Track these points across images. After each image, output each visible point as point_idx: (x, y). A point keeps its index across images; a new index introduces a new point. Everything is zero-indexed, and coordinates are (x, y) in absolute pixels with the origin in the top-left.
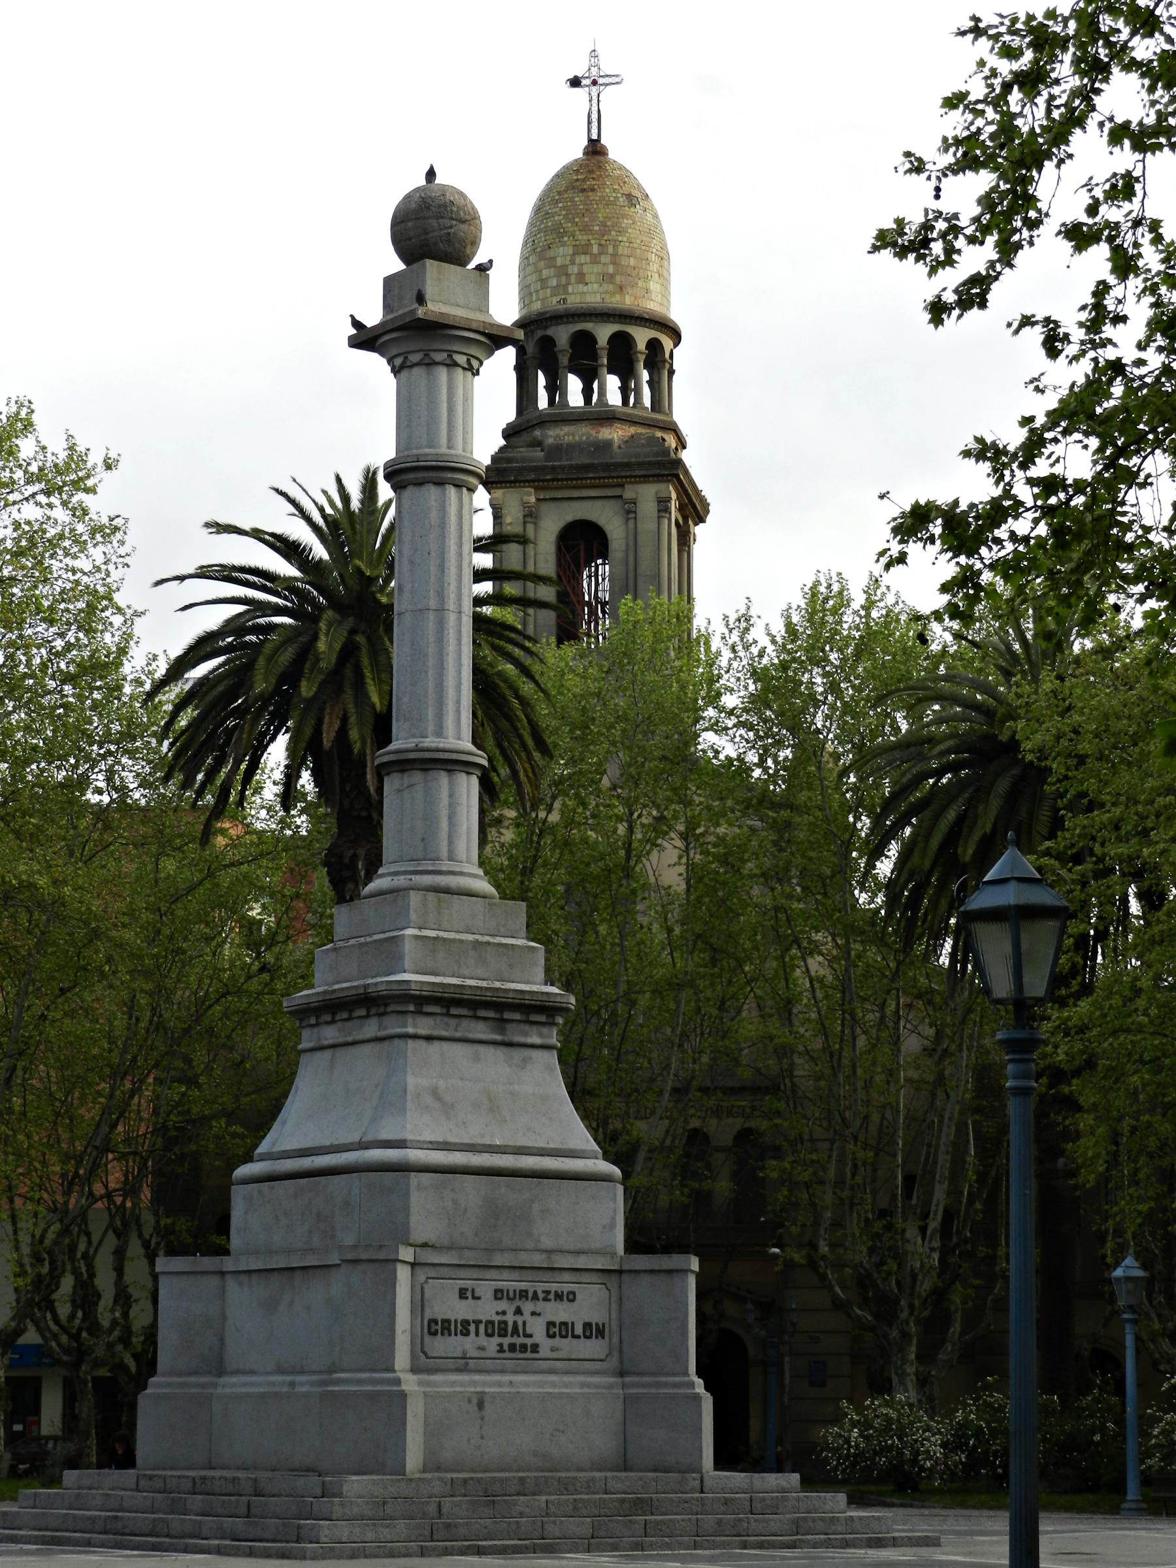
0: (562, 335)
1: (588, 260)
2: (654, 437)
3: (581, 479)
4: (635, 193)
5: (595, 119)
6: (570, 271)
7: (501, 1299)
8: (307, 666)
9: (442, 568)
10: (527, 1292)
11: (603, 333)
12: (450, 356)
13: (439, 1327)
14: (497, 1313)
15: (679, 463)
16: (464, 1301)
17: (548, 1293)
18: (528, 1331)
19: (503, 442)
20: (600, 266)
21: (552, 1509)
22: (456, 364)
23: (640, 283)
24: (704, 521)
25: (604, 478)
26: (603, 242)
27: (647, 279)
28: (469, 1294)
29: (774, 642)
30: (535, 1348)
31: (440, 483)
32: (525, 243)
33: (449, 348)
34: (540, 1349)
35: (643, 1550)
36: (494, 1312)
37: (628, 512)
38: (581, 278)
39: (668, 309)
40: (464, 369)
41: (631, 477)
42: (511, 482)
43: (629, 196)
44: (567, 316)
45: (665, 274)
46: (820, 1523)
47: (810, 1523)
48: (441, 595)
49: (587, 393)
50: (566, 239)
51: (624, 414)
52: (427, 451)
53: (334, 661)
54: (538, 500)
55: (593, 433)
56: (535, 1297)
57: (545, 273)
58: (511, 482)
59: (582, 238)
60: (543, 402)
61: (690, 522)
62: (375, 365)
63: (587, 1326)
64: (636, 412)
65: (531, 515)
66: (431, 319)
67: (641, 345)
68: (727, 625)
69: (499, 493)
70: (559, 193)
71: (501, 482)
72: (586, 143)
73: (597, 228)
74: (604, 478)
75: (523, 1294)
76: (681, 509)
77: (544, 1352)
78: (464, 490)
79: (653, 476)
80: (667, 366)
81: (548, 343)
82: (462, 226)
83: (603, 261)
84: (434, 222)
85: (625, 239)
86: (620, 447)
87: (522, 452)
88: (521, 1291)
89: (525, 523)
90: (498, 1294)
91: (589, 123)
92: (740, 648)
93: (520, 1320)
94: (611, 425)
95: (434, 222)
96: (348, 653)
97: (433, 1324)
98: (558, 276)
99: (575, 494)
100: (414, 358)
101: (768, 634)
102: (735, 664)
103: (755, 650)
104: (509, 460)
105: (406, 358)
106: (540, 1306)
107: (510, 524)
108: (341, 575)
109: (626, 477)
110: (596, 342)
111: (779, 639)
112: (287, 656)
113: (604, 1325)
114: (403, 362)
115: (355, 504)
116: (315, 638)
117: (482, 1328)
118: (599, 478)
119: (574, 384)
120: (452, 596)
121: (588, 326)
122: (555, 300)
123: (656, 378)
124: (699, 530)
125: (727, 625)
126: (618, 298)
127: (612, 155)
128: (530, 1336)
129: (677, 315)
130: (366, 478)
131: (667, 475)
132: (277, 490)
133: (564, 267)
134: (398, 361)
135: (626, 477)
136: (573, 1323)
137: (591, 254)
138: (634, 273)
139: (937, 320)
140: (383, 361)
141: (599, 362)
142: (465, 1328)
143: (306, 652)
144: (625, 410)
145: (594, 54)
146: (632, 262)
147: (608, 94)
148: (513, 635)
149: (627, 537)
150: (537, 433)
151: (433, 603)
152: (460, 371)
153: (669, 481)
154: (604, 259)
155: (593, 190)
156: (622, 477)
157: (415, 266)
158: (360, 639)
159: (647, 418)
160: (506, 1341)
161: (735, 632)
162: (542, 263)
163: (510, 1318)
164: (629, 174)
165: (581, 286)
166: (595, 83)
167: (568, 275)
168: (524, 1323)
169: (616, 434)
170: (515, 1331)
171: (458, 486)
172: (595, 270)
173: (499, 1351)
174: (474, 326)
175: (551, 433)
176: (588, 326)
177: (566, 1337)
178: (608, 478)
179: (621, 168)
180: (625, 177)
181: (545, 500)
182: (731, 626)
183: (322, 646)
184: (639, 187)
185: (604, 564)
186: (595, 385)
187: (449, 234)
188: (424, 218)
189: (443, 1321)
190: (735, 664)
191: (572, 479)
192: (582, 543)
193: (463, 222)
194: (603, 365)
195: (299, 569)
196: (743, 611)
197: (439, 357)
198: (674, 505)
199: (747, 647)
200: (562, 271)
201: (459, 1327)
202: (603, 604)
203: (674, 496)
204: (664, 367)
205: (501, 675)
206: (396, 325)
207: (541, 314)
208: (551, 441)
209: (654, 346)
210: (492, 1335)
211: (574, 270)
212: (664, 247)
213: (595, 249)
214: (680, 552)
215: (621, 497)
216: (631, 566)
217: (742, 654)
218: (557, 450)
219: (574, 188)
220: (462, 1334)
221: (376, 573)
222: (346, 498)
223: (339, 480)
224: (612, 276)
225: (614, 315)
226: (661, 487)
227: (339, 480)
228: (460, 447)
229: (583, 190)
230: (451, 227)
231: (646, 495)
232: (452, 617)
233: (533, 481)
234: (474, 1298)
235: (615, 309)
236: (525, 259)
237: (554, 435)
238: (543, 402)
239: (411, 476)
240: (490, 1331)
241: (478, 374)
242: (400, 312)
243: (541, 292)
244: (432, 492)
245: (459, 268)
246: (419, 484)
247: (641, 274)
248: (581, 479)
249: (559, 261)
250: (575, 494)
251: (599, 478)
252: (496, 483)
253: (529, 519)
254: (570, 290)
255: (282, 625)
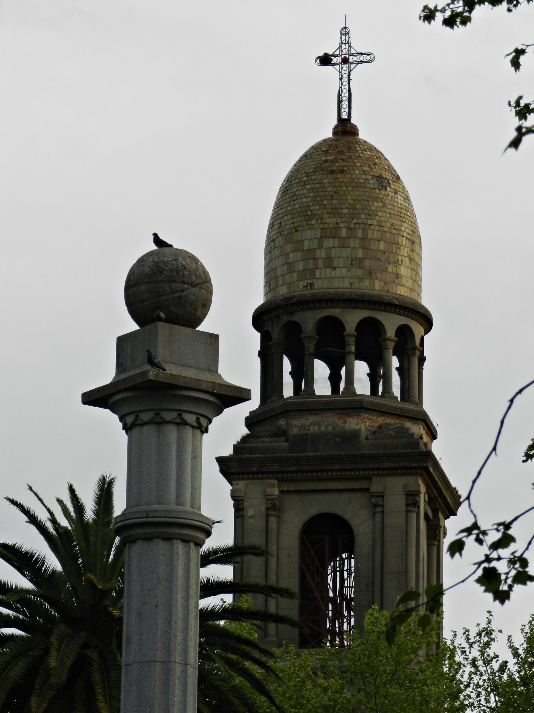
0: (309, 320)
1: (336, 245)
2: (402, 428)
3: (327, 471)
4: (387, 175)
5: (345, 98)
6: (317, 256)
8: (38, 681)
9: (169, 621)
11: (352, 319)
12: (180, 415)
15: (429, 456)
19: (246, 431)
20: (349, 250)
22: (185, 423)
23: (390, 268)
24: (455, 514)
25: (350, 470)
26: (352, 226)
27: (397, 263)
29: (516, 654)
31: (168, 539)
32: (272, 225)
33: (180, 408)
37: (375, 506)
38: (329, 263)
39: (419, 295)
40: (193, 427)
41: (378, 469)
42: (253, 473)
43: (380, 178)
44: (314, 301)
45: (416, 258)
48: (168, 647)
49: (334, 379)
50: (313, 222)
51: (372, 403)
52: (156, 507)
53: (65, 677)
54: (282, 492)
55: (340, 423)
57: (292, 257)
58: (253, 473)
59: (330, 221)
60: (288, 391)
61: (441, 516)
62: (108, 419)
64: (384, 401)
65: (274, 508)
66: (162, 380)
67: (391, 333)
68: (468, 639)
69: (241, 484)
70: (307, 174)
71: (243, 474)
72: (335, 122)
73: (345, 211)
74: (350, 470)
76: (431, 502)
78: (192, 545)
79: (402, 468)
80: (418, 353)
81: (294, 329)
82: (193, 289)
83: (352, 245)
84: (167, 287)
85: (375, 223)
86: (367, 438)
87: (266, 442)
89: (268, 516)
91: (340, 101)
92: (480, 663)
94: (359, 415)
95: (167, 287)
96: (80, 668)
98: (305, 260)
99: (320, 486)
100: (145, 417)
101: (510, 647)
102: (476, 679)
103: (496, 665)
104: (252, 451)
105: (137, 416)
107: (252, 517)
108: (74, 587)
109: (373, 469)
110: (344, 329)
111: (521, 651)
112: (17, 671)
114: (135, 421)
115: (89, 514)
116: (46, 652)
118: (345, 470)
119: (321, 370)
120: (179, 649)
121: (336, 312)
122: (302, 284)
123: (406, 365)
125: (468, 639)
126: (367, 283)
127: (362, 135)
129: (427, 301)
130: (101, 488)
131: (416, 468)
132: (13, 502)
133: (311, 250)
134: (130, 420)
135: (373, 469)
137: (340, 238)
138: (384, 258)
139: (488, 612)
140: (115, 418)
141: (347, 349)
143: (37, 667)
144: (375, 400)
145: (345, 31)
146: (382, 246)
147: (358, 72)
148: (248, 649)
149: (374, 532)
150: (282, 422)
151: (160, 656)
152: (189, 429)
153: (417, 474)
154: (353, 243)
155: (342, 172)
156: (369, 470)
157: (147, 327)
158: (93, 654)
159: (396, 408)
161: (476, 646)
162: (289, 247)
164: (379, 155)
165: (328, 270)
166: (345, 61)
167: (315, 259)
169: (362, 424)
171: (186, 541)
172: (344, 255)
174: (203, 386)
175: (296, 422)
176: (336, 312)
178: (355, 470)
179: (372, 148)
180: (374, 157)
181: (288, 492)
182: (472, 640)
183: (52, 662)
184: (390, 169)
185: (349, 558)
186: (343, 372)
187: (180, 297)
188: (158, 282)
190: (476, 679)
191: (317, 471)
192: (327, 537)
193: (194, 285)
194: (350, 353)
195: (31, 581)
196: (484, 625)
197: (169, 416)
198: (423, 499)
199: (487, 662)
200: (309, 255)
202: (349, 601)
203: (423, 489)
204: (414, 354)
205: (235, 690)
206: (128, 385)
207: (287, 299)
208: (295, 431)
209: (404, 332)
211: (321, 254)
212: (415, 231)
213: (344, 233)
214: (429, 546)
215: (367, 490)
216: (378, 563)
217: (482, 669)
218: (302, 440)
219: (322, 169)
221: (108, 586)
222: (79, 508)
223: (72, 490)
224: (361, 261)
225: (363, 301)
226: (411, 479)
227: (72, 490)
228: (188, 503)
229: (332, 172)
230: (183, 291)
231: (394, 488)
232: (178, 668)
233: (277, 472)
235: (363, 295)
236: (271, 242)
237: (298, 425)
238: (288, 391)
239: (140, 531)
241: (207, 431)
242: (133, 373)
243: (287, 276)
244: (160, 546)
245: (189, 330)
246: (148, 539)
247: (391, 260)
248: (327, 471)
249: (307, 245)
250: (320, 486)
251: (345, 470)
252: (238, 474)
253: (272, 512)
254: (317, 275)
255: (12, 637)
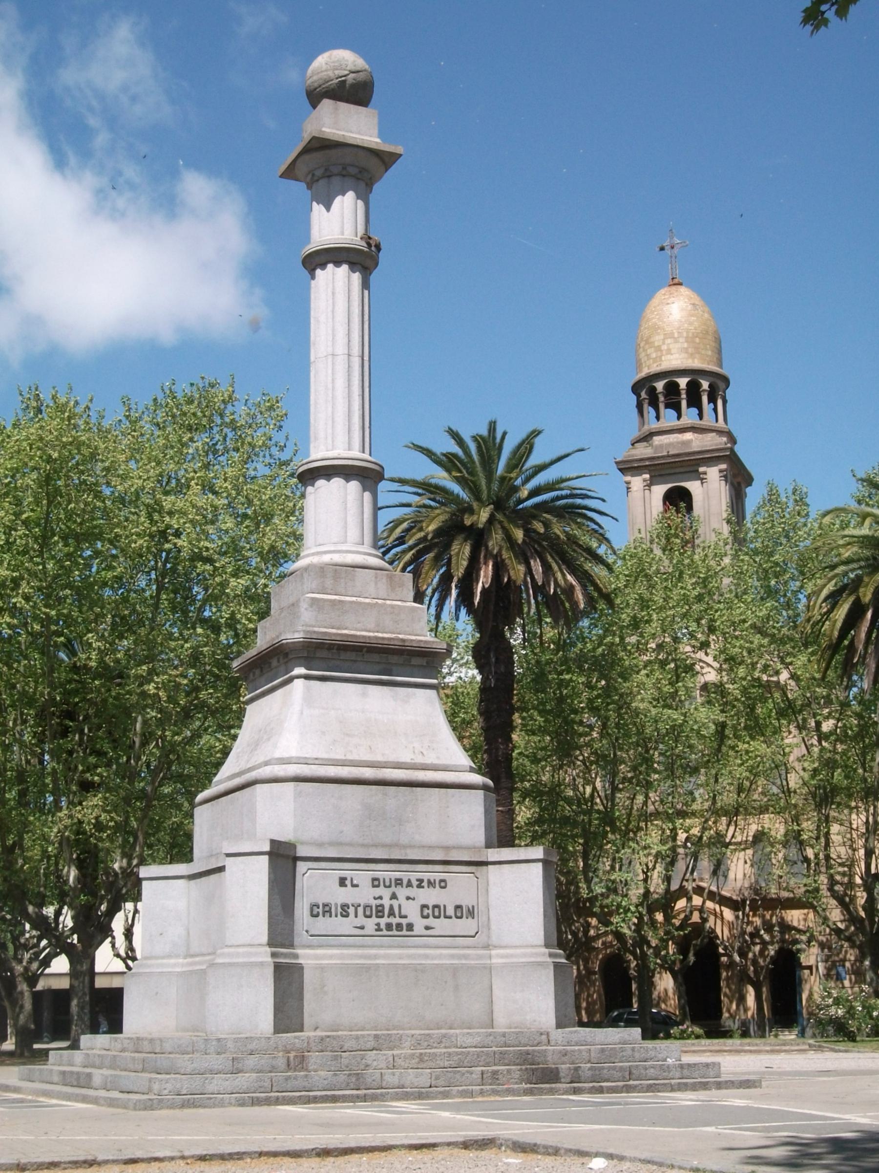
7: (378, 886)
10: (401, 880)
11: (683, 382)
13: (320, 910)
14: (375, 898)
16: (343, 888)
17: (421, 881)
18: (403, 913)
21: (399, 1062)
28: (348, 882)
30: (410, 927)
34: (414, 928)
35: (472, 1097)
36: (371, 897)
38: (669, 351)
46: (652, 1070)
47: (642, 1071)
56: (409, 884)
63: (458, 907)
75: (399, 882)
77: (418, 929)
81: (652, 392)
88: (396, 880)
90: (375, 882)
93: (395, 903)
97: (315, 908)
99: (672, 471)
106: (413, 892)
113: (473, 907)
117: (360, 910)
124: (748, 490)
128: (406, 917)
136: (445, 906)
142: (344, 910)
160: (383, 921)
163: (386, 902)
167: (661, 351)
168: (400, 906)
170: (392, 913)
173: (376, 930)
177: (439, 917)
189: (325, 905)
201: (339, 910)
210: (370, 917)
220: (342, 916)
234: (354, 886)
240: (437, 914)
